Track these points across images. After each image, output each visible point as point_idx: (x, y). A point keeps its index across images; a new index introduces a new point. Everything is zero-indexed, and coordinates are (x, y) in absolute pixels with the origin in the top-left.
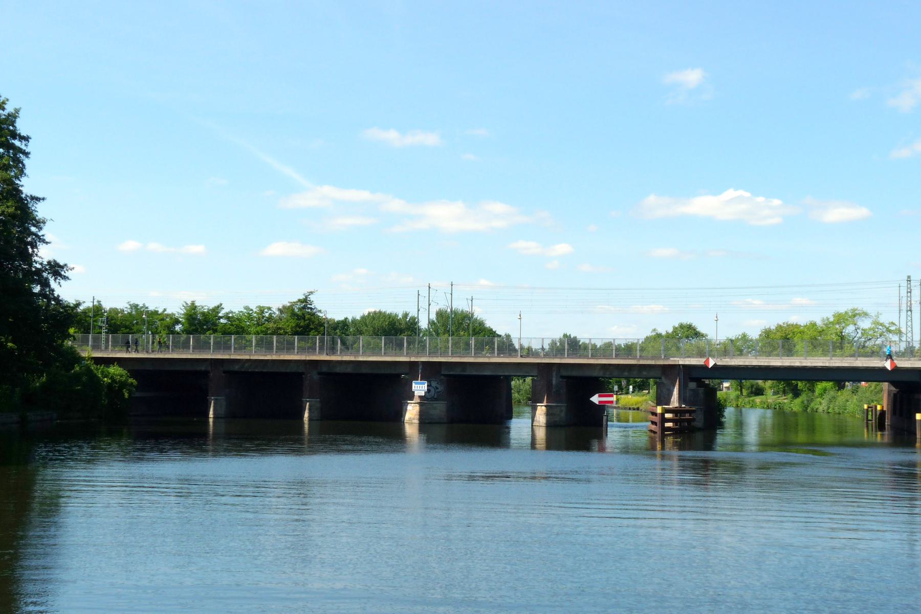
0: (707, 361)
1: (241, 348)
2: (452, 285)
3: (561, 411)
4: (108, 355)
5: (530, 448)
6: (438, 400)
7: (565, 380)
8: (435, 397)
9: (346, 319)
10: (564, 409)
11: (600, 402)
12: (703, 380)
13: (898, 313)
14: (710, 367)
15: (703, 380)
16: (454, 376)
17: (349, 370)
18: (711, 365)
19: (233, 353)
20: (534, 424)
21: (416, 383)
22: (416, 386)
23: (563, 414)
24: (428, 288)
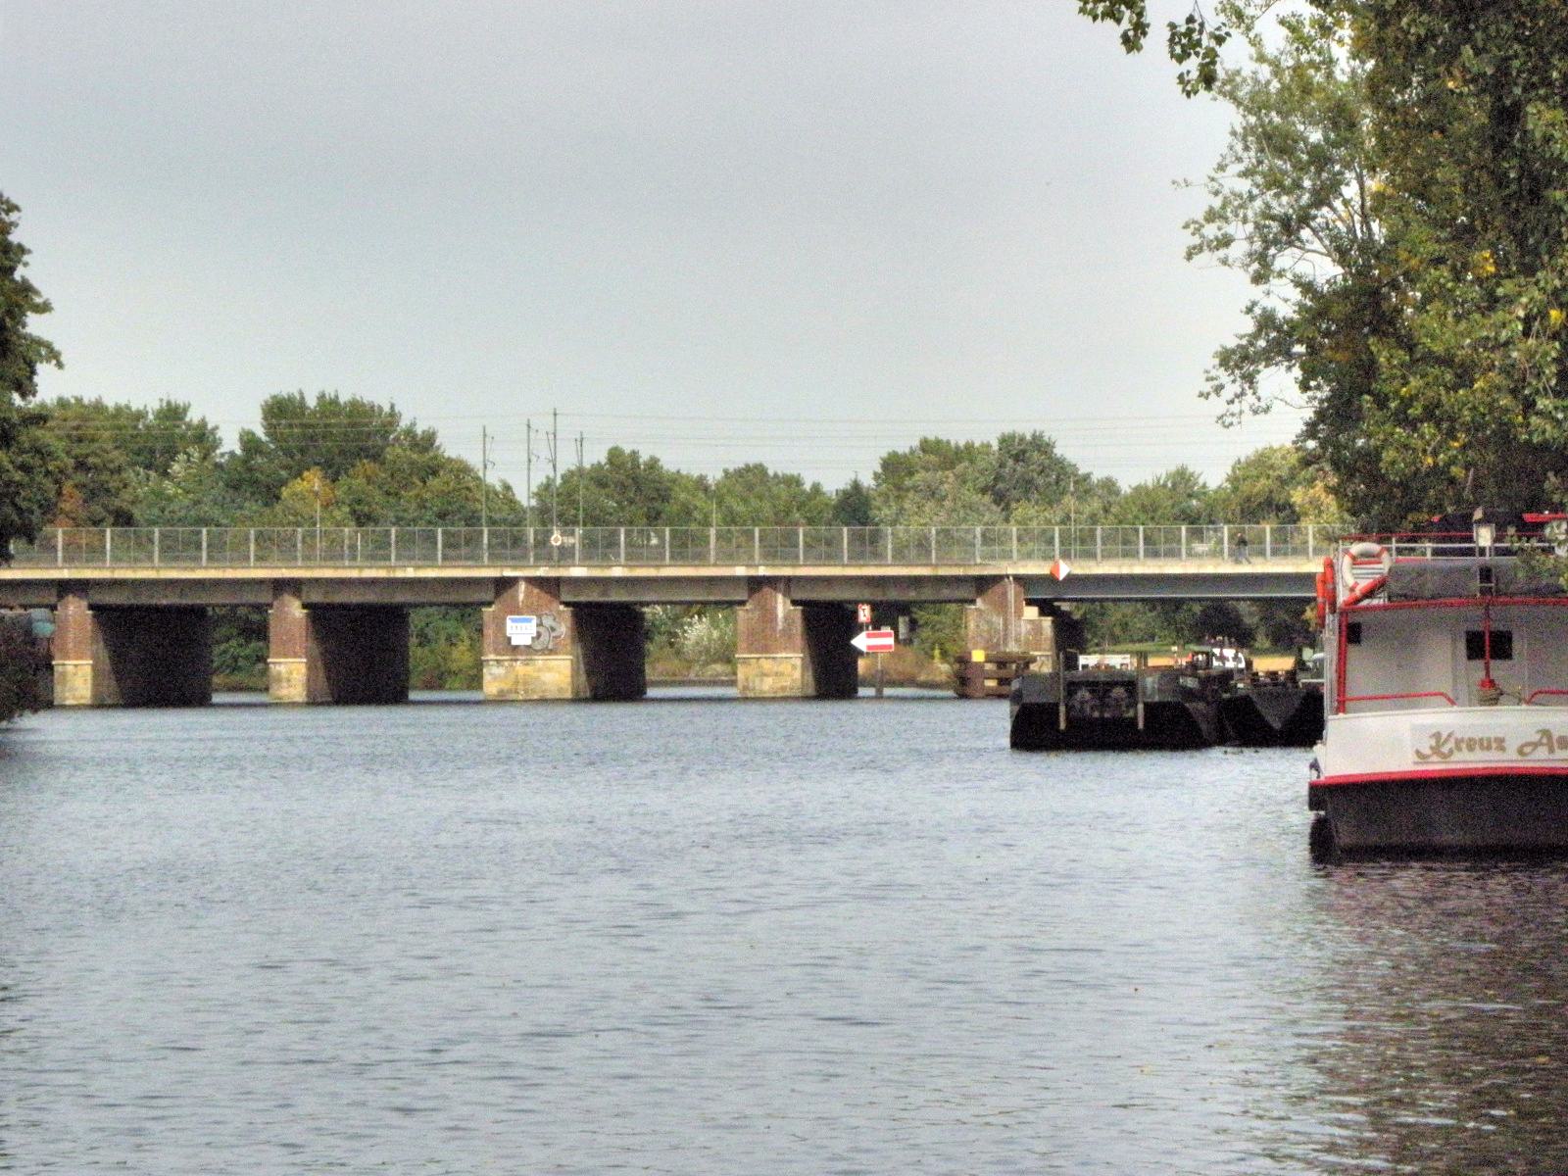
0: (1057, 567)
1: (1283, 546)
2: (555, 415)
3: (794, 667)
4: (1199, 566)
5: (1006, 741)
6: (556, 654)
7: (800, 608)
8: (550, 647)
9: (856, 486)
10: (799, 663)
11: (869, 647)
12: (1056, 604)
13: (526, 472)
14: (1061, 578)
15: (1056, 604)
16: (589, 605)
17: (370, 597)
18: (1062, 576)
19: (667, 561)
20: (1349, 694)
21: (513, 621)
22: (514, 625)
23: (797, 674)
24: (526, 428)
